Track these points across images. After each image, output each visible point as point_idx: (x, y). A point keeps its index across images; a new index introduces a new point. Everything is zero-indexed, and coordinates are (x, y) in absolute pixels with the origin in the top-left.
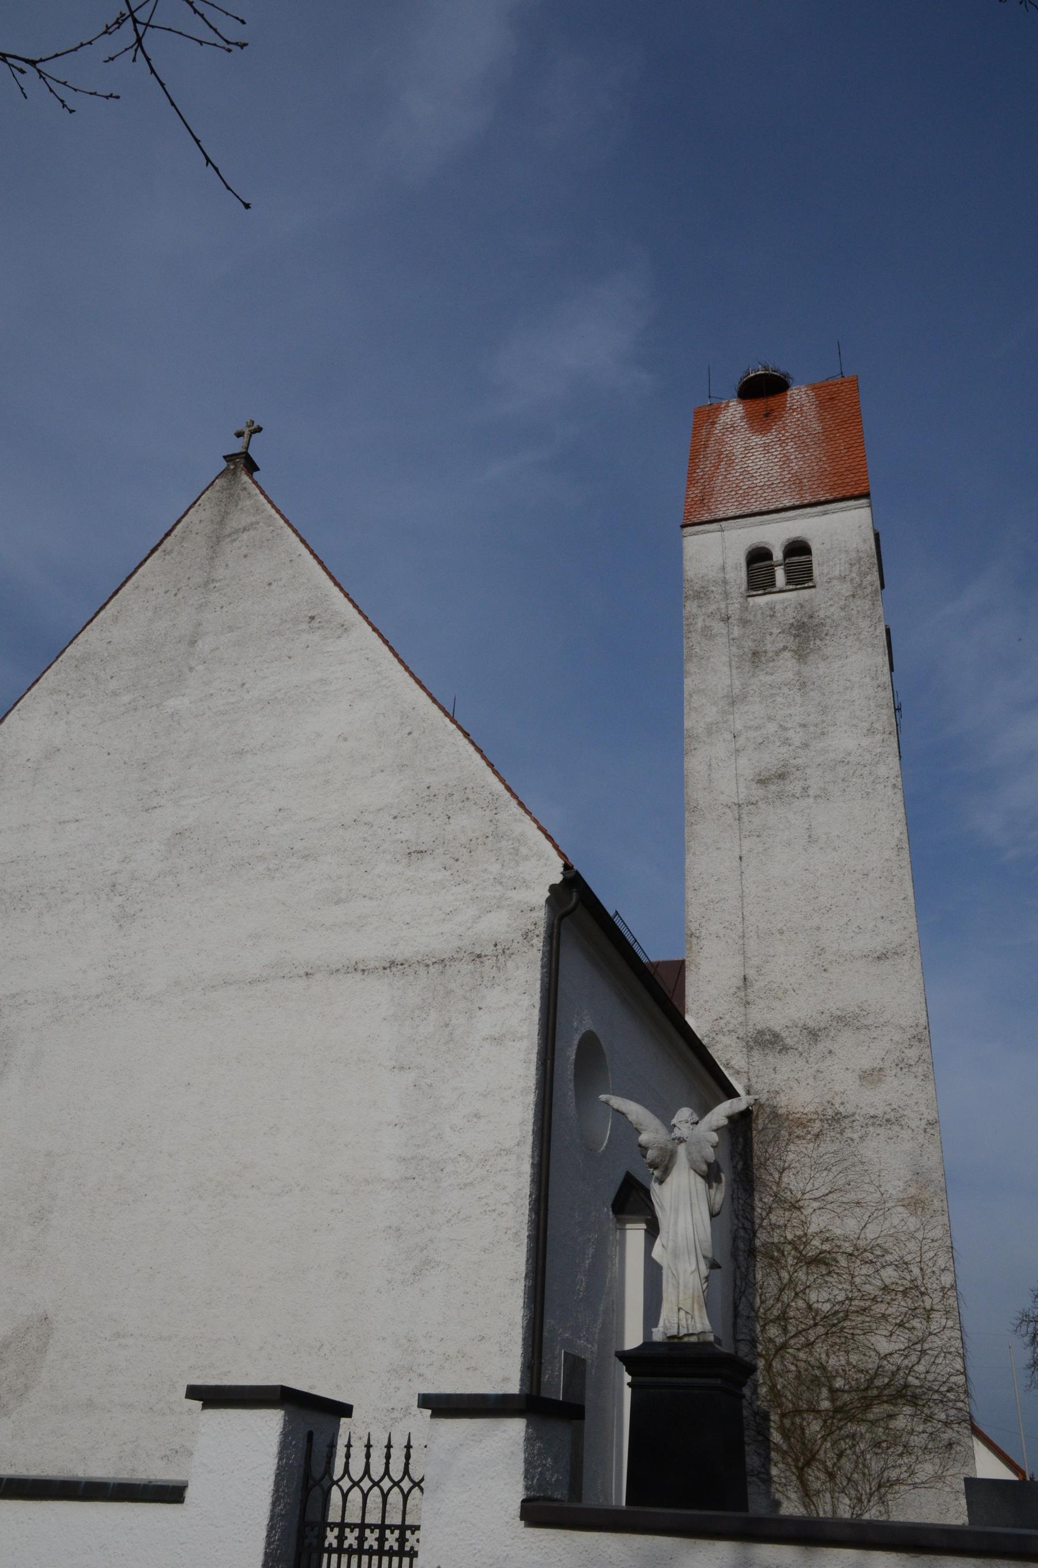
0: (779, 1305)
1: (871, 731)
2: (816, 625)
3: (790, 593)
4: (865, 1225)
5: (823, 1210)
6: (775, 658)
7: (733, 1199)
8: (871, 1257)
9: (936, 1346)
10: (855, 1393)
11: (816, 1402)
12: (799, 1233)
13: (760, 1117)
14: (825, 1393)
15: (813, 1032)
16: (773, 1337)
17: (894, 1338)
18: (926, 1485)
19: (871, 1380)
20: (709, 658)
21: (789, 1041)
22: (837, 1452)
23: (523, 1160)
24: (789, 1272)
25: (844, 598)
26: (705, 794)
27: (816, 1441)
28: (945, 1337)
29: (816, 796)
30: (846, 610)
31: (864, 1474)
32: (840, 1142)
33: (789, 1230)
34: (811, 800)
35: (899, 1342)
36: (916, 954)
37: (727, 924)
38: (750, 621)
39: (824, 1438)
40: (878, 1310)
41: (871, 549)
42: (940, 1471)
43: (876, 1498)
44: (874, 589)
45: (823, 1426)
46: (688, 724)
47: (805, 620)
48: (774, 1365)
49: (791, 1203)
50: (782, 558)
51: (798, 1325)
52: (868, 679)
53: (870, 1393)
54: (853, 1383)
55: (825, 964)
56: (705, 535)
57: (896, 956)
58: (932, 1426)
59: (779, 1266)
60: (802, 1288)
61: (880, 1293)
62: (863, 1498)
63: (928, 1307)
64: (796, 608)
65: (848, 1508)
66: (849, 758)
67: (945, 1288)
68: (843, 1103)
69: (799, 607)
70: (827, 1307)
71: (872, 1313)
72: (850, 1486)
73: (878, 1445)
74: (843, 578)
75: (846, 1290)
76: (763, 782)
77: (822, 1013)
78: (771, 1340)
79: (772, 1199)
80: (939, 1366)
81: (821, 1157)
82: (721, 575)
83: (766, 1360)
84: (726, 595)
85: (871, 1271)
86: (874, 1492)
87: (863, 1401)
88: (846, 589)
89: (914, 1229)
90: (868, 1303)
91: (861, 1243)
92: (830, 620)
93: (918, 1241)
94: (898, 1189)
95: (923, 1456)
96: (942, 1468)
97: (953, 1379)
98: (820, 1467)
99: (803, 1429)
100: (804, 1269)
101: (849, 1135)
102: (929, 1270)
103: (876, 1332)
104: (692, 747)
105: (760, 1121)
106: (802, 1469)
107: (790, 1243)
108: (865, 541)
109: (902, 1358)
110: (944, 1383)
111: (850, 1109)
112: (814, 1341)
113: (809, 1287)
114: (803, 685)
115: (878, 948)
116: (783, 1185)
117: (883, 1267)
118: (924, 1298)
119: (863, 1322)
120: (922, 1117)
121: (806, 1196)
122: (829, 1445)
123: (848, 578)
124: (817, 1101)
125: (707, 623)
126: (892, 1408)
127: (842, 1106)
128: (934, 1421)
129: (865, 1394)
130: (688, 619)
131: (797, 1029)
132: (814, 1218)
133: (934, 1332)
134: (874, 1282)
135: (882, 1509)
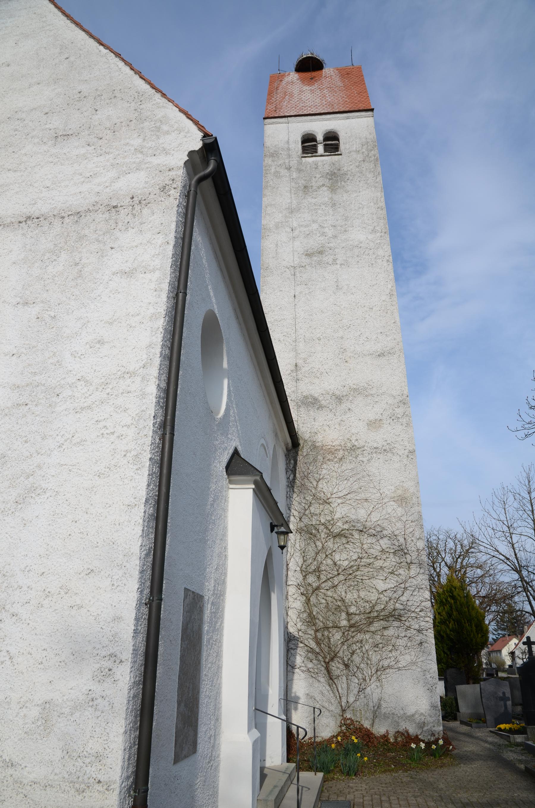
0: (315, 563)
1: (374, 231)
2: (342, 174)
3: (327, 157)
4: (370, 514)
5: (344, 504)
6: (318, 190)
7: (287, 497)
8: (374, 532)
9: (413, 584)
10: (363, 615)
11: (338, 622)
12: (329, 518)
13: (305, 447)
14: (344, 615)
15: (338, 398)
16: (311, 582)
17: (388, 580)
18: (406, 668)
19: (373, 606)
20: (278, 188)
21: (323, 403)
22: (351, 652)
23: (148, 381)
24: (322, 542)
25: (358, 162)
26: (274, 260)
27: (337, 646)
28: (419, 579)
29: (341, 264)
30: (360, 167)
31: (367, 664)
32: (355, 463)
33: (322, 516)
34: (338, 266)
35: (391, 583)
36: (401, 354)
37: (285, 334)
38: (303, 170)
39: (343, 643)
40: (378, 564)
41: (374, 138)
42: (415, 659)
43: (375, 678)
44: (375, 158)
45: (342, 636)
46: (264, 222)
47: (336, 171)
48: (312, 600)
49: (324, 500)
50: (322, 139)
51: (327, 575)
52: (372, 204)
53: (372, 615)
54: (362, 609)
55: (346, 358)
56: (277, 125)
57: (389, 355)
58: (410, 633)
59: (316, 539)
60: (330, 552)
61: (380, 554)
62: (367, 678)
63: (409, 562)
64: (330, 165)
65: (357, 685)
66: (361, 245)
67: (419, 549)
68: (357, 440)
69: (332, 164)
70: (346, 563)
71: (374, 566)
72: (358, 671)
73: (376, 646)
74: (358, 152)
75: (358, 553)
76: (309, 255)
77: (345, 386)
78: (310, 584)
79: (312, 497)
80: (415, 597)
81: (343, 472)
82: (286, 146)
83: (306, 597)
84: (289, 156)
85: (374, 541)
86: (374, 674)
87: (367, 620)
88: (360, 157)
89: (400, 515)
90: (372, 560)
91: (368, 524)
92: (350, 172)
93: (403, 522)
94: (391, 491)
95: (404, 651)
96: (416, 657)
97: (423, 604)
98: (340, 661)
99: (329, 639)
100: (332, 540)
101: (361, 459)
102: (410, 539)
103: (377, 577)
104: (266, 234)
105: (305, 450)
106: (328, 662)
107: (323, 524)
108: (370, 134)
109: (393, 593)
110: (418, 606)
111: (361, 443)
112: (337, 585)
113: (334, 551)
114: (334, 205)
115: (379, 350)
116: (319, 489)
117: (382, 538)
118: (406, 556)
119: (369, 572)
120: (406, 448)
121: (334, 496)
122: (346, 647)
123: (361, 152)
124: (341, 438)
125: (277, 170)
126: (386, 623)
127: (356, 442)
128: (411, 629)
129: (369, 615)
130: (266, 167)
131: (328, 396)
132: (338, 509)
133: (412, 576)
134: (376, 547)
135: (378, 684)
